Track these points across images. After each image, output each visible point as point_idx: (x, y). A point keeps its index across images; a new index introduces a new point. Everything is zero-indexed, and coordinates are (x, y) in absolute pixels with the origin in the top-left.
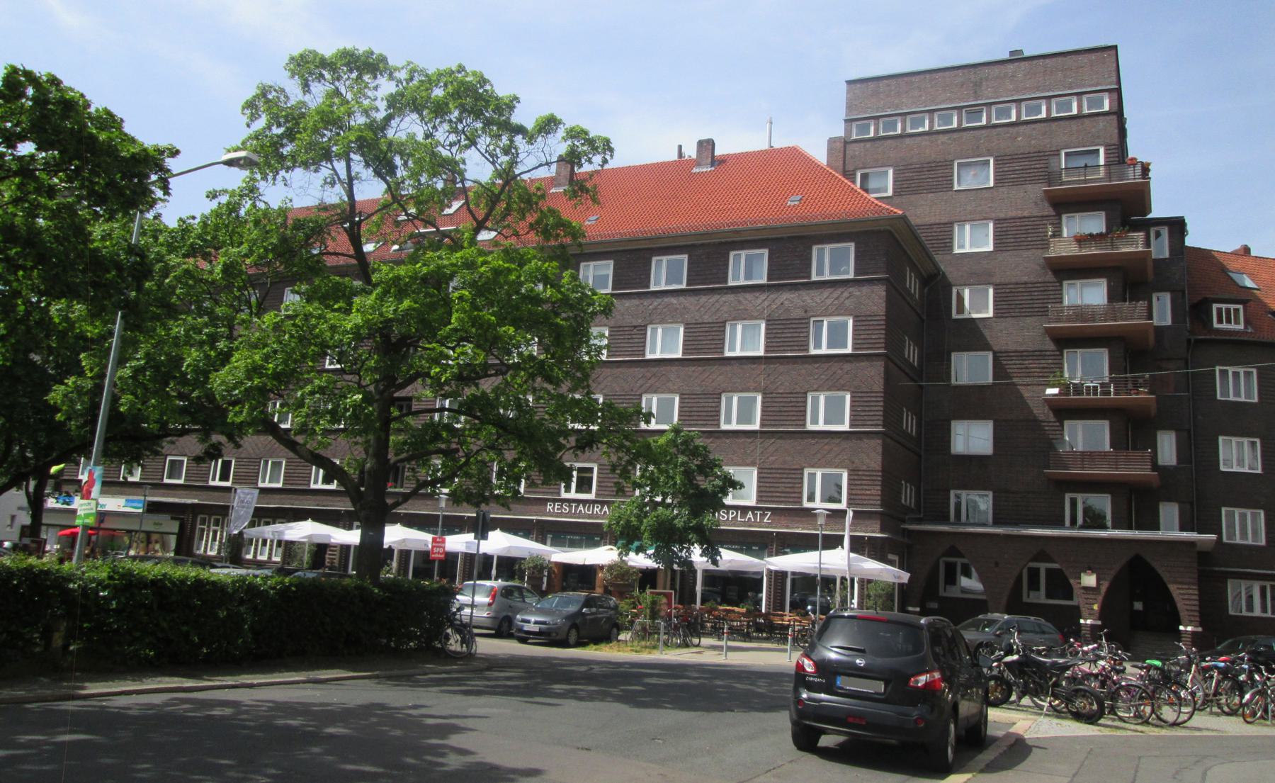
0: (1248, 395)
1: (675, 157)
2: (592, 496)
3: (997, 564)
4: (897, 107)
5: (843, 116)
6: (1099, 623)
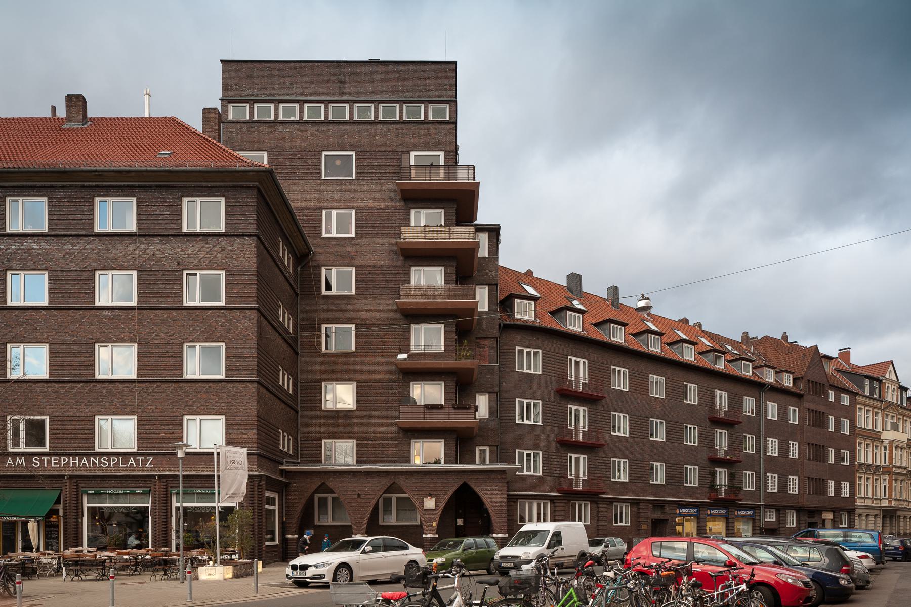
0: (535, 369)
1: (49, 115)
2: (46, 449)
3: (359, 495)
5: (220, 97)
6: (437, 536)
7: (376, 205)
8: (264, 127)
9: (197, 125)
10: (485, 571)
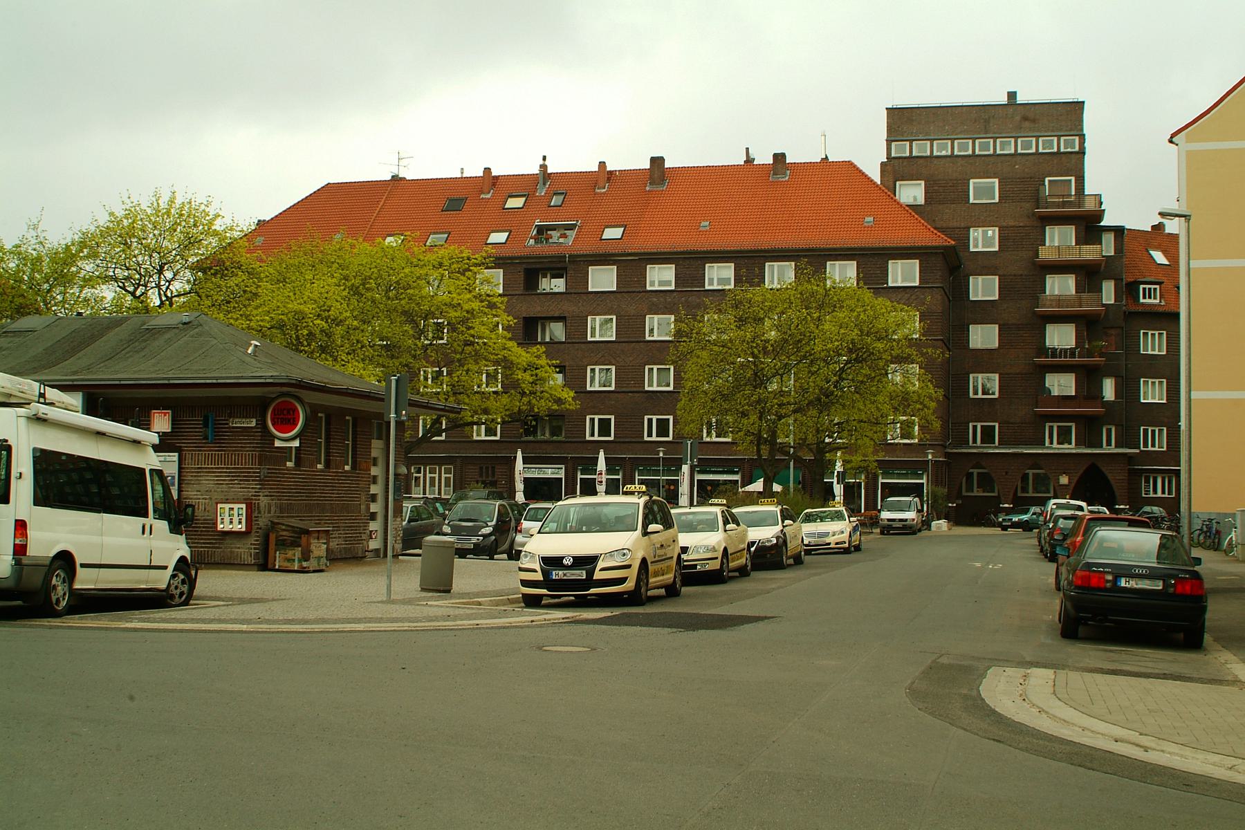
4: (927, 134)
7: (1017, 224)
8: (921, 161)
9: (876, 176)
10: (505, 556)
